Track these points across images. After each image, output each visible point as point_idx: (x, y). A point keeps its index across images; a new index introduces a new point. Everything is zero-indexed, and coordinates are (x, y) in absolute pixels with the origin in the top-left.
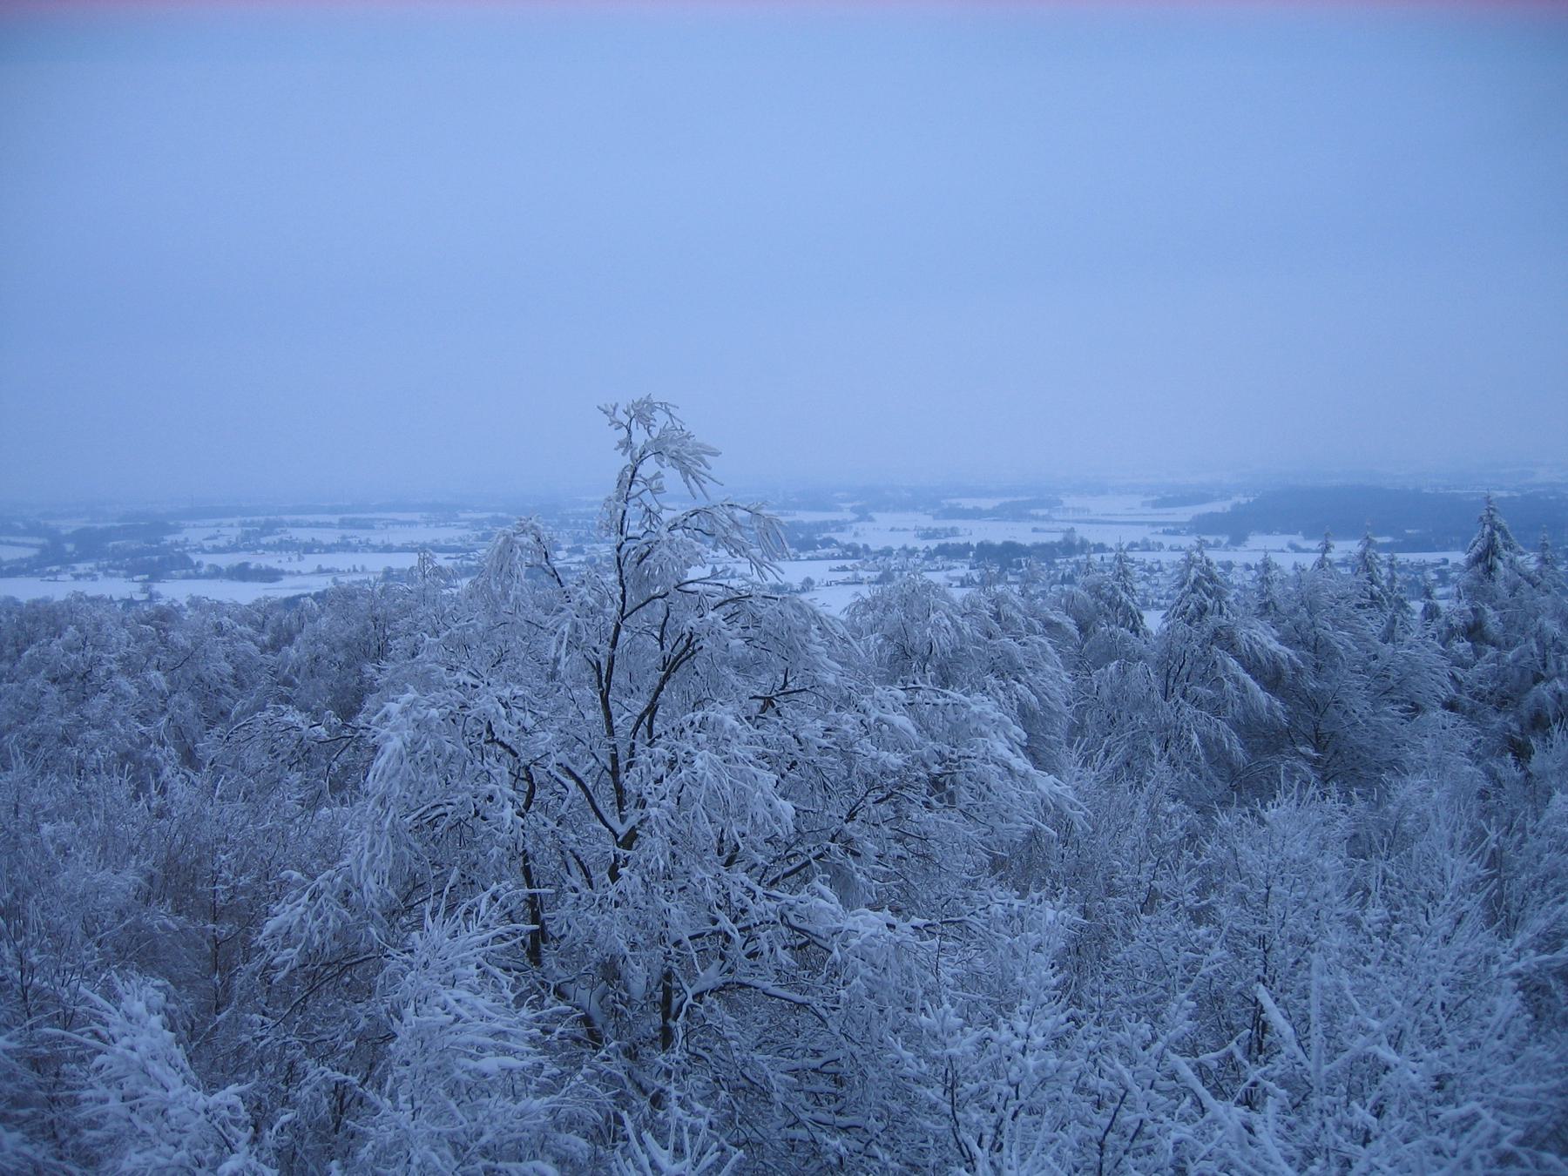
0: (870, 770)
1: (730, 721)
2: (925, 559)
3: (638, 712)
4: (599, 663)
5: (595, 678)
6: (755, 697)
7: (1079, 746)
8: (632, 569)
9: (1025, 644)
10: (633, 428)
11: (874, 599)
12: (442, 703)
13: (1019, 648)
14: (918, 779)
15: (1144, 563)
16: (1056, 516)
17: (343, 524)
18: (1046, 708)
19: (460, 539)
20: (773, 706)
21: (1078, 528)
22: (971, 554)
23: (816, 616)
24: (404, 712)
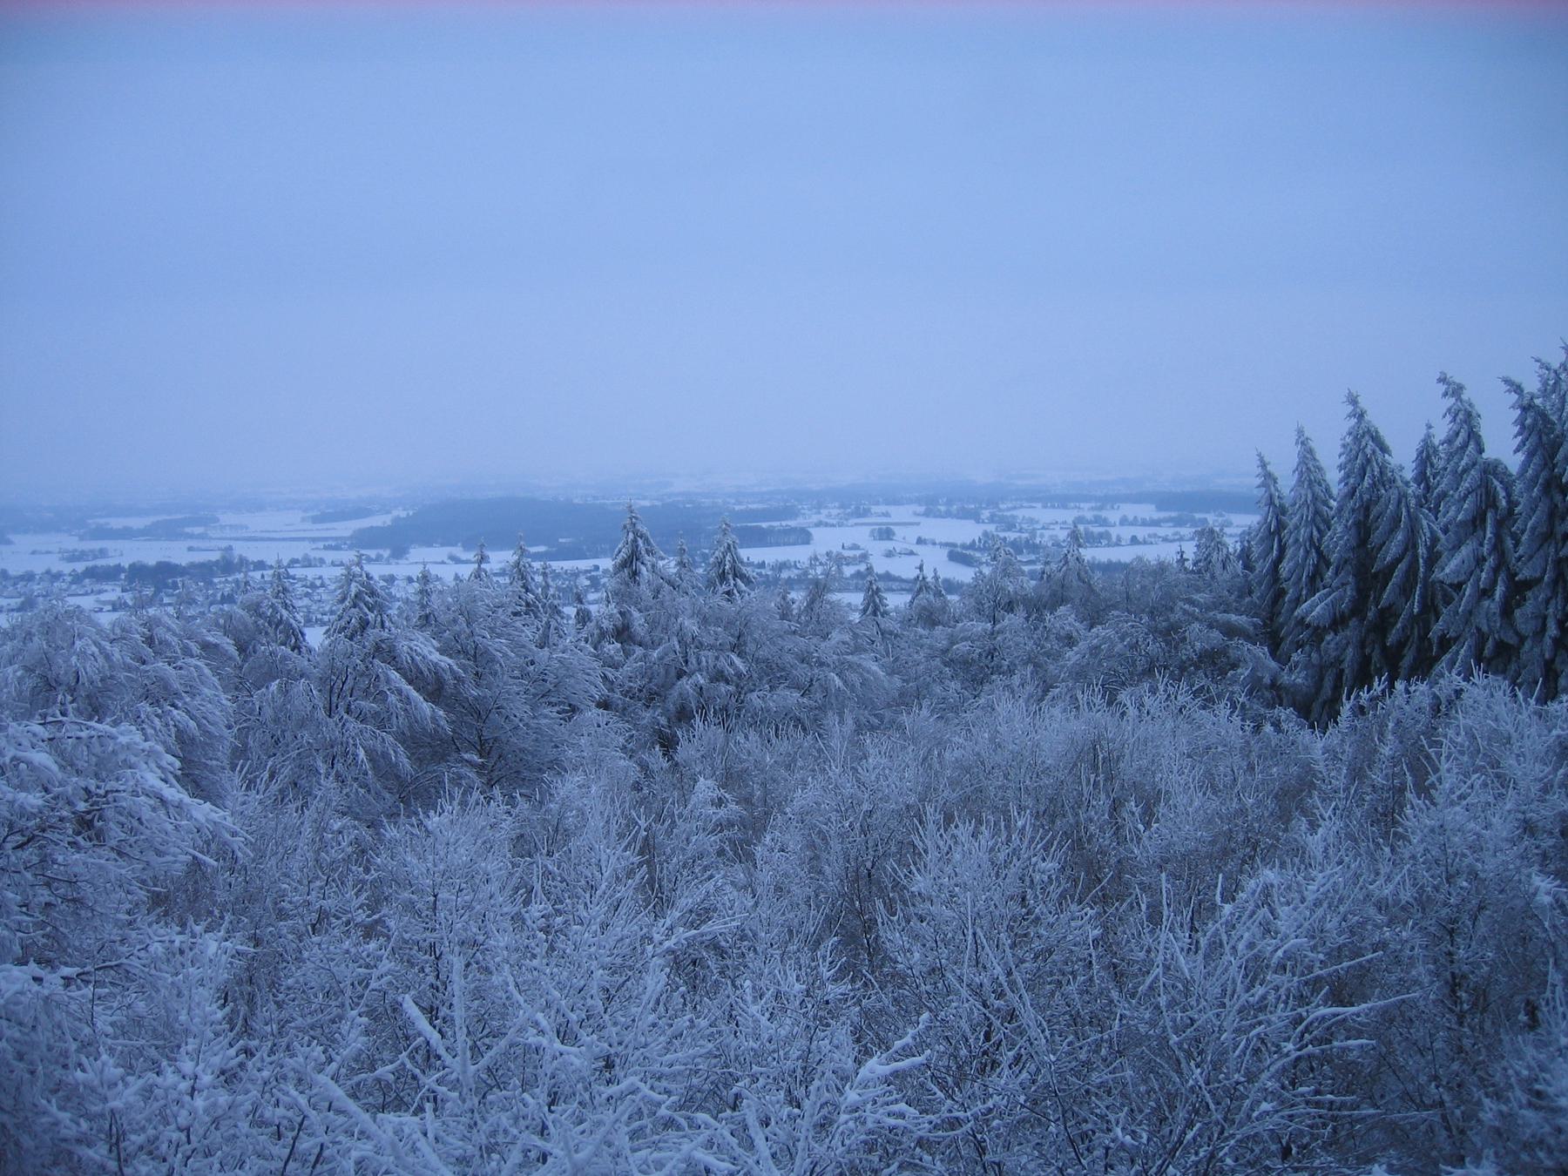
2: (72, 583)
13: (174, 672)
14: (62, 819)
15: (305, 579)
18: (206, 733)
22: (123, 576)
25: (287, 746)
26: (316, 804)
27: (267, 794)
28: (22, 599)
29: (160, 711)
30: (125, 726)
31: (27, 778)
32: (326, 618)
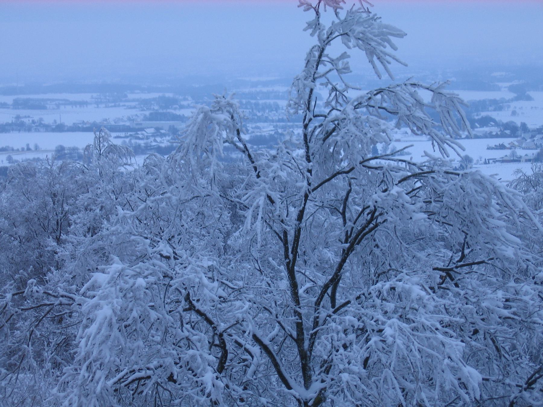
1: (417, 291)
4: (285, 233)
5: (282, 252)
8: (318, 146)
10: (321, 10)
11: (536, 175)
12: (146, 273)
17: (17, 105)
19: (129, 119)
23: (497, 192)
24: (113, 282)
28: (538, 150)
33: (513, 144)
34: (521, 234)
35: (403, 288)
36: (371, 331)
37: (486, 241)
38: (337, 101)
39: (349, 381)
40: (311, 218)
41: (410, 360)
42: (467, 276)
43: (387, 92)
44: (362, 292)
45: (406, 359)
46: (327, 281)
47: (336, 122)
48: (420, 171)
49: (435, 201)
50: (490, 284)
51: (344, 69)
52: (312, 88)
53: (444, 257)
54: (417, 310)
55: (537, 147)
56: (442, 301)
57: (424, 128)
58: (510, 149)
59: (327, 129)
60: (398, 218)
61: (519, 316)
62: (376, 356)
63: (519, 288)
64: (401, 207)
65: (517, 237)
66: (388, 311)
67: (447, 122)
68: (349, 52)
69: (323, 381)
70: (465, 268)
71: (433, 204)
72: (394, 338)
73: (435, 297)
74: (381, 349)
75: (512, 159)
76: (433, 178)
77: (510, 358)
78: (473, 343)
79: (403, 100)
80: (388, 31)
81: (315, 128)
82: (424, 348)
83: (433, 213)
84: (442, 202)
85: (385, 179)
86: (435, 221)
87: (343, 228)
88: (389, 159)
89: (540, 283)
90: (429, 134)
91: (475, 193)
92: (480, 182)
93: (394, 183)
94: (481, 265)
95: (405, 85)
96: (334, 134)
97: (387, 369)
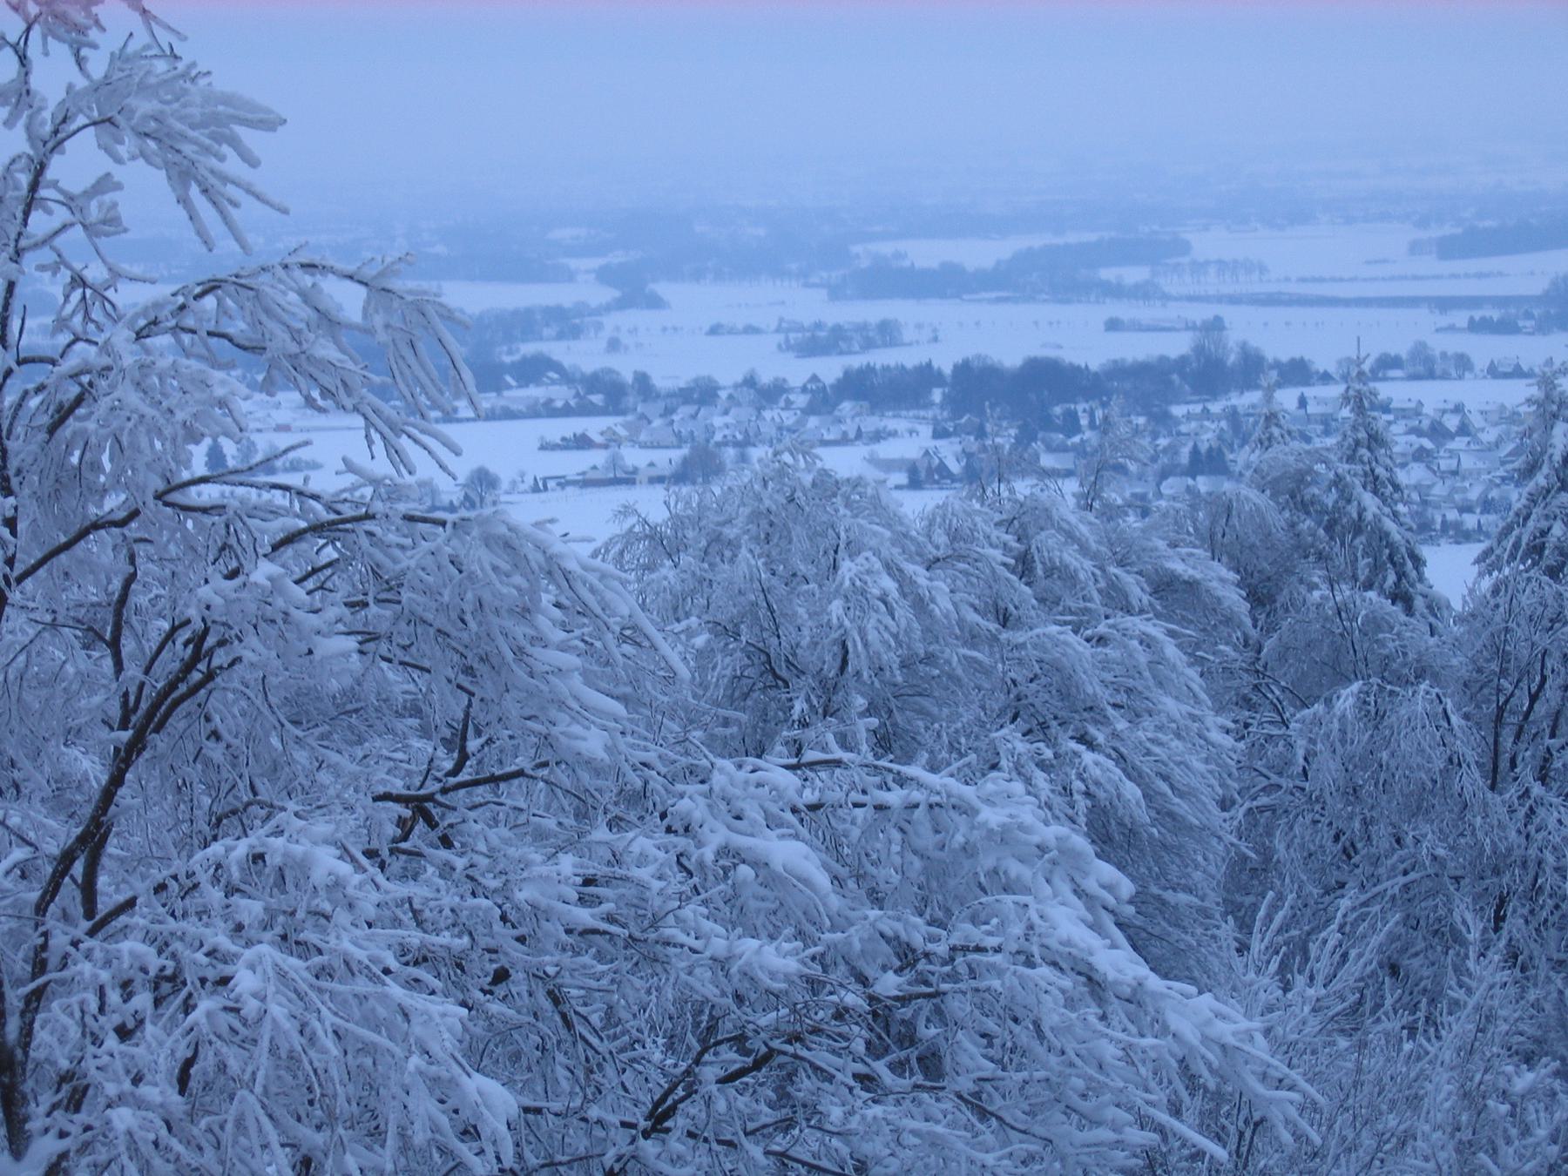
0: (710, 991)
1: (327, 862)
2: (810, 410)
3: (53, 848)
6: (387, 797)
7: (1269, 918)
8: (34, 447)
9: (1101, 640)
10: (34, 50)
11: (678, 522)
13: (1086, 650)
14: (841, 1014)
15: (1417, 412)
16: (1171, 285)
18: (1166, 816)
20: (432, 824)
21: (1228, 313)
22: (937, 395)
23: (555, 570)
25: (1376, 862)
26: (1459, 1027)
27: (1336, 985)
28: (685, 451)
29: (1048, 754)
30: (993, 783)
31: (753, 904)
32: (1470, 521)
33: (614, 433)
34: (628, 690)
35: (286, 855)
36: (198, 984)
37: (528, 712)
38: (87, 317)
39: (135, 1129)
40: (22, 658)
41: (311, 1063)
42: (472, 814)
43: (232, 288)
44: (172, 871)
45: (299, 1061)
46: (70, 842)
47: (85, 379)
48: (333, 516)
49: (378, 601)
50: (540, 836)
51: (104, 222)
52: (13, 278)
53: (409, 762)
54: (328, 918)
55: (680, 440)
56: (399, 890)
57: (341, 391)
58: (606, 447)
59: (59, 397)
60: (274, 654)
61: (623, 926)
62: (211, 1053)
63: (619, 846)
64: (280, 622)
65: (617, 698)
66: (246, 923)
67: (407, 372)
68: (119, 173)
69: (63, 1135)
70: (480, 789)
71: (374, 609)
72: (263, 999)
73: (380, 879)
74: (225, 1031)
75: (611, 475)
76: (370, 534)
77: (603, 1047)
78: (495, 1007)
79: (279, 310)
80: (231, 111)
81: (25, 395)
82: (350, 1026)
83: (374, 637)
84: (399, 602)
85: (233, 541)
86: (378, 658)
87: (114, 686)
88: (241, 484)
89: (681, 831)
90: (356, 409)
91: (493, 576)
92: (507, 545)
93: (260, 551)
94: (516, 782)
95: (286, 267)
96: (81, 411)
97: (245, 1092)
